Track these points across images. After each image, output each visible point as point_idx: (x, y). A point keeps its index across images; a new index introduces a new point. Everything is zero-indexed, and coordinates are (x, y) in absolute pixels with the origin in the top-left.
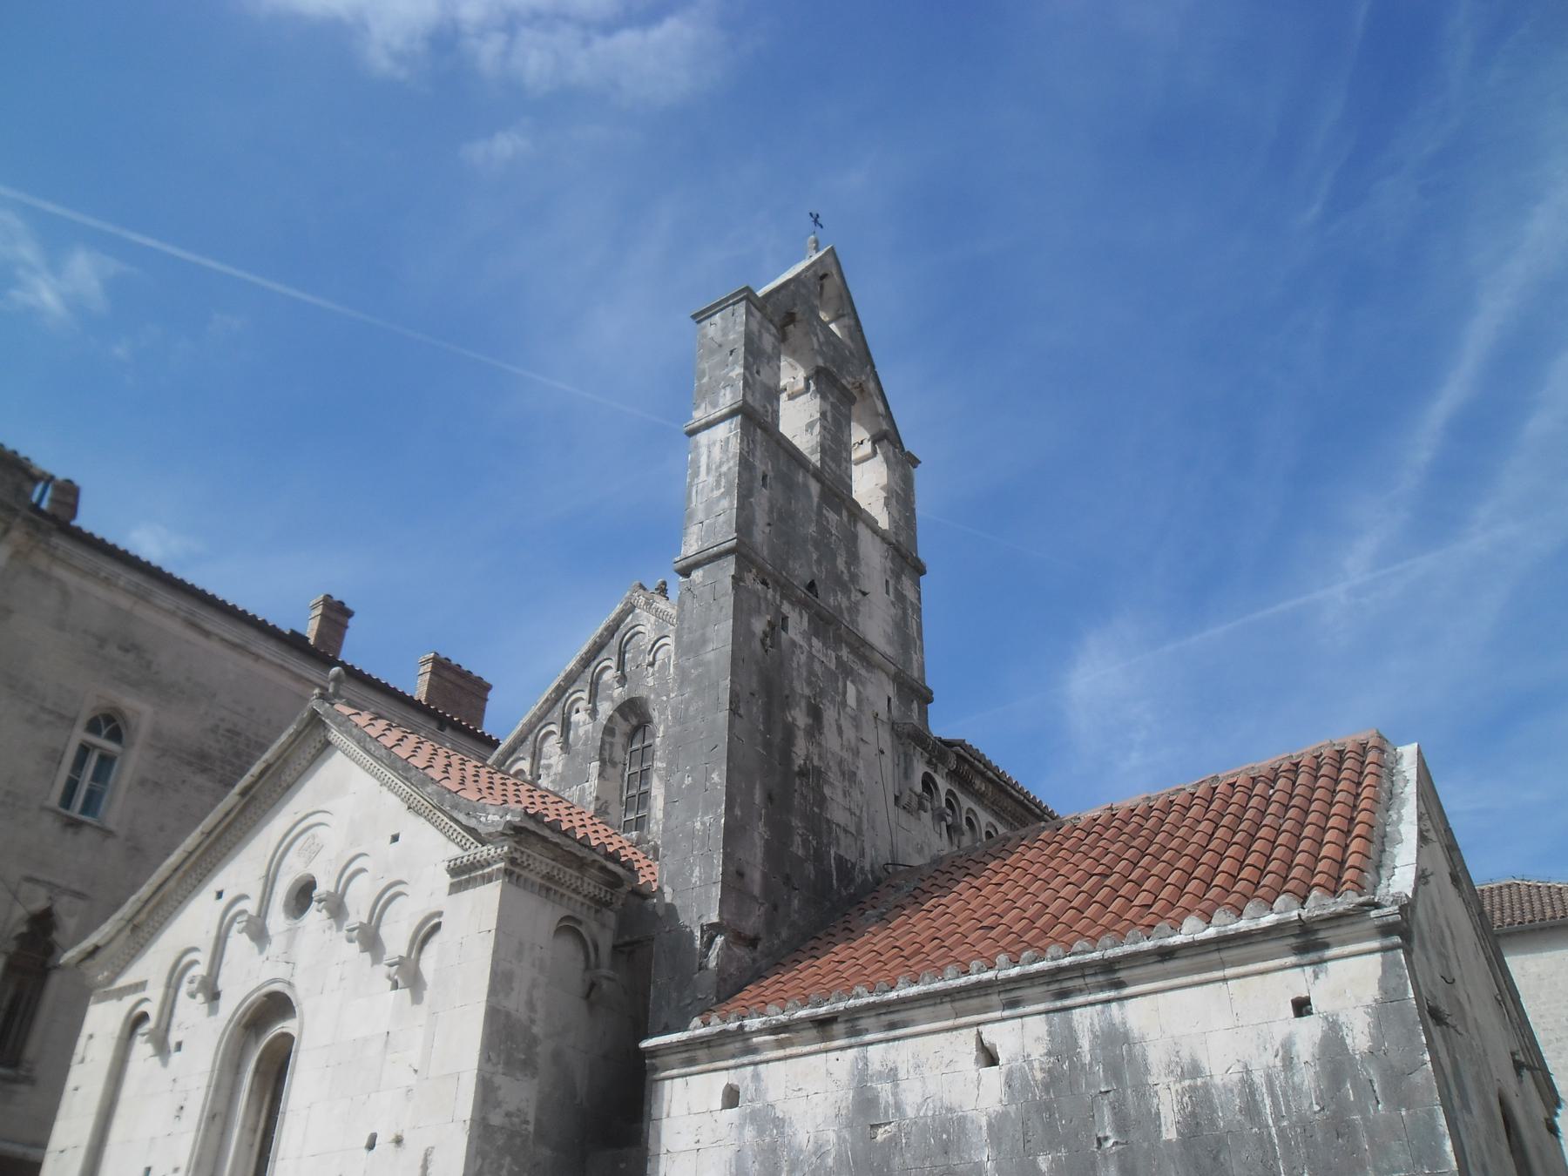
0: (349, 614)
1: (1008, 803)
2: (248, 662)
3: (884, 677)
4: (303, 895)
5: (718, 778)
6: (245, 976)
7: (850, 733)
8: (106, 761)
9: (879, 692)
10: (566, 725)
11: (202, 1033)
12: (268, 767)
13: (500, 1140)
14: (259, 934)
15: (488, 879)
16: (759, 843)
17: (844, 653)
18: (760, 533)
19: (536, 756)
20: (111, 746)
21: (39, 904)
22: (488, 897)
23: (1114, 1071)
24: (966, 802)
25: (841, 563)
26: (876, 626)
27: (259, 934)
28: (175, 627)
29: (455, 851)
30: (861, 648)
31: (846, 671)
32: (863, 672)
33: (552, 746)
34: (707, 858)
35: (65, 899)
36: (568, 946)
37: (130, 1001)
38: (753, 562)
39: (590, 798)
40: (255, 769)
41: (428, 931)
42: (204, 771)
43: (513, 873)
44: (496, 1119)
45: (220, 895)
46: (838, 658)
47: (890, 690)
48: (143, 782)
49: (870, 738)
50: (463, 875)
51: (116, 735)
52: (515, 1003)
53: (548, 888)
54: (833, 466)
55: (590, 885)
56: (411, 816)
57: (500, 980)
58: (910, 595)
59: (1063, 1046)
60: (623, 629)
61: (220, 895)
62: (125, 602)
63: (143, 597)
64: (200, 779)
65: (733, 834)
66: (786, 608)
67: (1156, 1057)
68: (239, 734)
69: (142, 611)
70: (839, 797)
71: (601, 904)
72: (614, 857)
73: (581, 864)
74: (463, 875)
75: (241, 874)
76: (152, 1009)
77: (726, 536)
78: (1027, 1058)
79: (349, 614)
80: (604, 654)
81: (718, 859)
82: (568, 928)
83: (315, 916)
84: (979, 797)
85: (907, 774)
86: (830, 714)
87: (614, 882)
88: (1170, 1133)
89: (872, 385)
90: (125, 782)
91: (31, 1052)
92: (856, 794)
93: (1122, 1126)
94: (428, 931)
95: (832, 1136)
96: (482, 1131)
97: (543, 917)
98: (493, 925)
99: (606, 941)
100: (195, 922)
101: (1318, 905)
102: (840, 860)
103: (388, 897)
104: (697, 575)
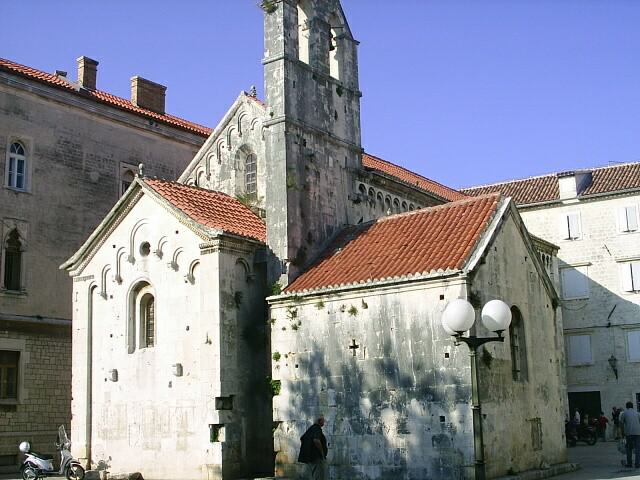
0: (96, 63)
1: (396, 186)
2: (67, 109)
3: (344, 150)
4: (146, 248)
5: (284, 210)
6: (131, 276)
7: (330, 177)
8: (21, 163)
9: (342, 155)
10: (219, 155)
11: (121, 294)
12: (123, 202)
13: (228, 328)
14: (132, 260)
15: (213, 251)
16: (299, 229)
17: (328, 146)
18: (293, 111)
19: (208, 165)
20: (21, 157)
21: (13, 227)
22: (215, 256)
23: (396, 311)
24: (377, 190)
25: (326, 107)
26: (340, 130)
27: (132, 260)
28: (34, 98)
29: (201, 241)
30: (335, 142)
31: (328, 153)
32: (336, 151)
33: (214, 161)
34: (282, 236)
35: (21, 224)
36: (240, 267)
37: (89, 282)
38: (291, 123)
39: (232, 185)
40: (118, 203)
41: (195, 265)
42: (59, 161)
43: (221, 249)
44: (226, 323)
45: (114, 247)
46: (326, 149)
47: (346, 153)
48: (37, 170)
49: (338, 176)
50: (206, 249)
51: (21, 152)
52: (227, 289)
53: (232, 251)
54: (322, 63)
55: (245, 247)
56: (180, 224)
57: (222, 283)
58: (355, 108)
59: (384, 306)
60: (238, 112)
61: (114, 247)
62: (12, 91)
63: (22, 89)
64: (58, 166)
65: (290, 227)
66: (305, 136)
67: (406, 308)
68: (68, 143)
69: (19, 94)
70: (327, 203)
71: (248, 252)
72: (252, 238)
73: (241, 242)
74: (206, 249)
75: (120, 235)
76: (98, 281)
77: (282, 54)
78: (375, 307)
79: (96, 63)
80: (231, 123)
81: (286, 238)
82: (240, 261)
83: (152, 256)
84: (383, 187)
85: (353, 187)
86: (323, 173)
87: (252, 245)
88: (408, 327)
89: (338, 12)
90: (30, 172)
91: (23, 284)
92: (333, 201)
93: (397, 325)
94: (195, 265)
95: (323, 328)
96: (223, 326)
97: (232, 260)
98: (217, 266)
99: (251, 263)
100: (104, 255)
101: (449, 272)
102: (328, 226)
103: (177, 253)
104: (271, 128)
